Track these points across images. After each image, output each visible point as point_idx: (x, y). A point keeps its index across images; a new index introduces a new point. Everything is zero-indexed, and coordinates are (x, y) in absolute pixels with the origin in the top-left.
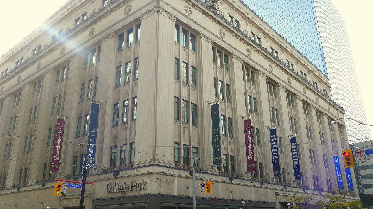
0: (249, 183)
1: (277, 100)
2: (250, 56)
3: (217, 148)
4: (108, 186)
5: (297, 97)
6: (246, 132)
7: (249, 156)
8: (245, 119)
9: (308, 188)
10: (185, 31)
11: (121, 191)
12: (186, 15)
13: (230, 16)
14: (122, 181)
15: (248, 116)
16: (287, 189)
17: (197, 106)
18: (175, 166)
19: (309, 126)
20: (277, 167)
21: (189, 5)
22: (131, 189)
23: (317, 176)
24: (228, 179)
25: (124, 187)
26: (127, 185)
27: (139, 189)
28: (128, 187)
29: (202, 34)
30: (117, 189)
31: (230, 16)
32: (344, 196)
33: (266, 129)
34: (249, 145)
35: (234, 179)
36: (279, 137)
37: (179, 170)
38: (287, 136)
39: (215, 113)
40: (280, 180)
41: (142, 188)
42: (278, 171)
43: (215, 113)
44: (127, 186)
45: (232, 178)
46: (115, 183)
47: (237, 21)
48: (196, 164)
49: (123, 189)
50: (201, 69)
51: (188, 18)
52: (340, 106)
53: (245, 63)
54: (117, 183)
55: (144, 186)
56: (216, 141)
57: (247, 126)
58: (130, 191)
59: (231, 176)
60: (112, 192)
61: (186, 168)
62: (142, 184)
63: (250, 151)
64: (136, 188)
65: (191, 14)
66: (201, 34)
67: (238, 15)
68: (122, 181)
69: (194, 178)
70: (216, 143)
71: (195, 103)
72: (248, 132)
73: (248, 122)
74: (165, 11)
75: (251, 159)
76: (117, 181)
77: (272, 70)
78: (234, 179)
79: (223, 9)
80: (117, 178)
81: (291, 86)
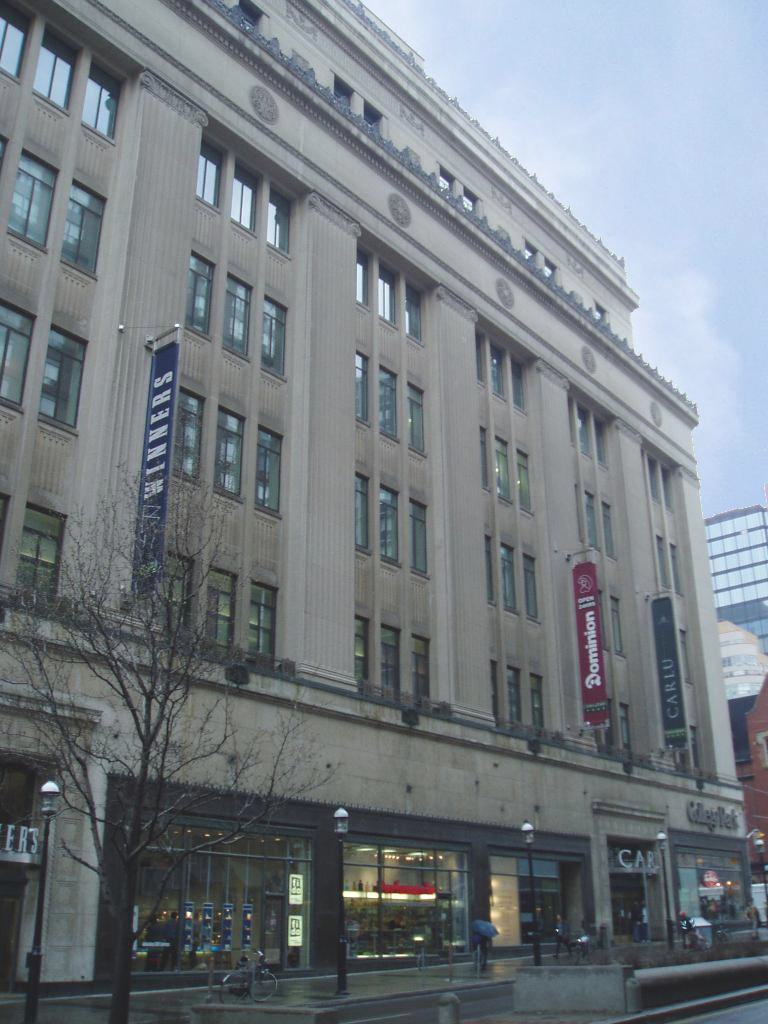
0: (666, 779)
2: (593, 371)
3: (672, 706)
5: (619, 425)
6: (581, 600)
7: (592, 676)
8: (576, 561)
9: (713, 779)
10: (390, 277)
12: (501, 304)
13: (529, 247)
15: (584, 552)
16: (704, 791)
18: (355, 690)
19: (669, 540)
20: (673, 716)
21: (589, 347)
24: (620, 765)
29: (149, 71)
31: (529, 247)
32: (700, 785)
33: (640, 599)
34: (590, 642)
35: (545, 748)
36: (681, 630)
38: (640, 599)
39: (663, 619)
40: (684, 757)
42: (678, 731)
43: (663, 619)
45: (629, 763)
47: (549, 264)
50: (687, 549)
51: (262, 129)
52: (390, 142)
53: (647, 447)
56: (670, 688)
57: (583, 582)
59: (410, 704)
61: (391, 698)
63: (592, 661)
65: (273, 117)
66: (681, 466)
67: (603, 288)
70: (671, 694)
72: (586, 602)
73: (585, 570)
74: (551, 368)
75: (595, 686)
77: (659, 423)
78: (545, 748)
79: (282, 29)
81: (512, 317)
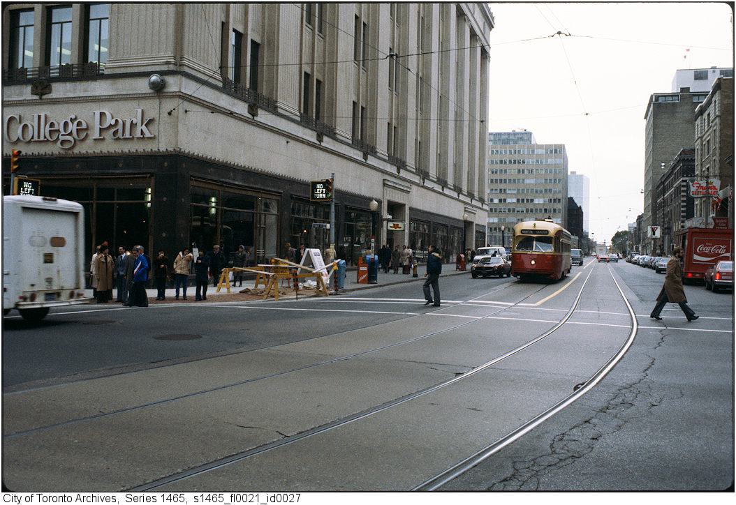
1: (325, 42)
4: (13, 126)
11: (61, 138)
14: (59, 115)
17: (261, 47)
22: (97, 136)
23: (318, 82)
25: (73, 127)
26: (83, 122)
27: (127, 135)
28: (87, 129)
30: (45, 130)
37: (91, 22)
41: (139, 135)
44: (84, 126)
46: (31, 115)
48: (53, 95)
49: (70, 134)
54: (46, 116)
55: (144, 127)
58: (95, 139)
60: (29, 142)
62: (137, 120)
64: (115, 133)
68: (59, 115)
69: (38, 8)
71: (258, 40)
76: (44, 111)
80: (41, 102)
